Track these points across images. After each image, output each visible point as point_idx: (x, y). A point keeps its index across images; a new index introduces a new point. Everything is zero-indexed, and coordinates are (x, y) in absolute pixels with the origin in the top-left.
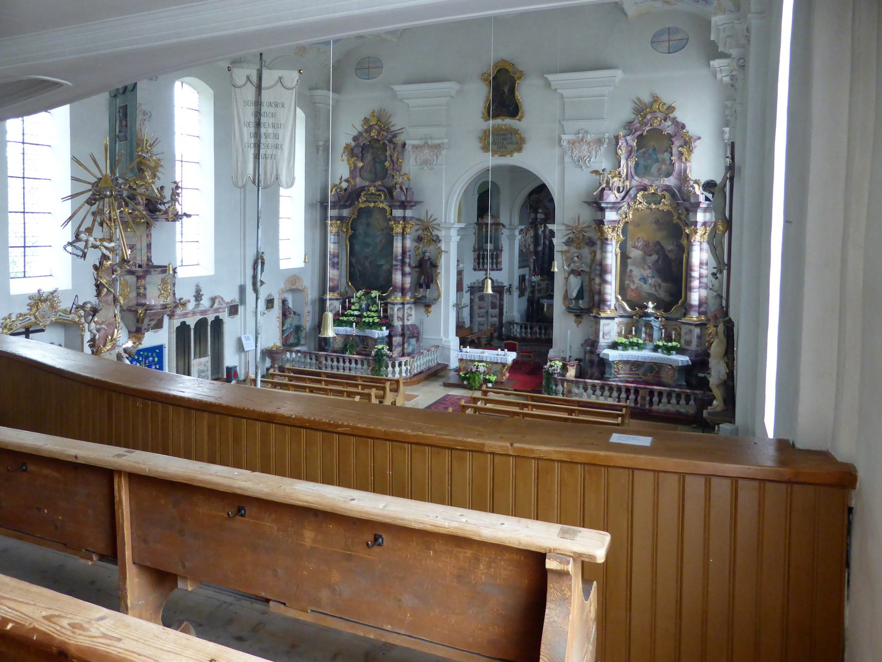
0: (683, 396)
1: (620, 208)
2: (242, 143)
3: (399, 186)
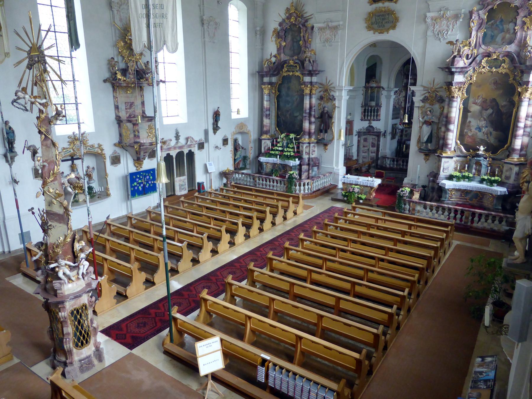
0: (497, 218)
1: (467, 72)
2: (137, 14)
3: (308, 59)
